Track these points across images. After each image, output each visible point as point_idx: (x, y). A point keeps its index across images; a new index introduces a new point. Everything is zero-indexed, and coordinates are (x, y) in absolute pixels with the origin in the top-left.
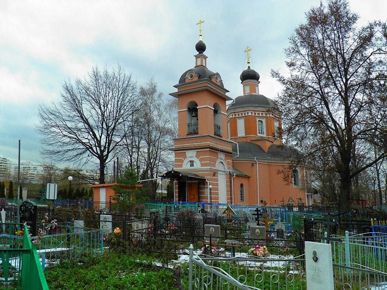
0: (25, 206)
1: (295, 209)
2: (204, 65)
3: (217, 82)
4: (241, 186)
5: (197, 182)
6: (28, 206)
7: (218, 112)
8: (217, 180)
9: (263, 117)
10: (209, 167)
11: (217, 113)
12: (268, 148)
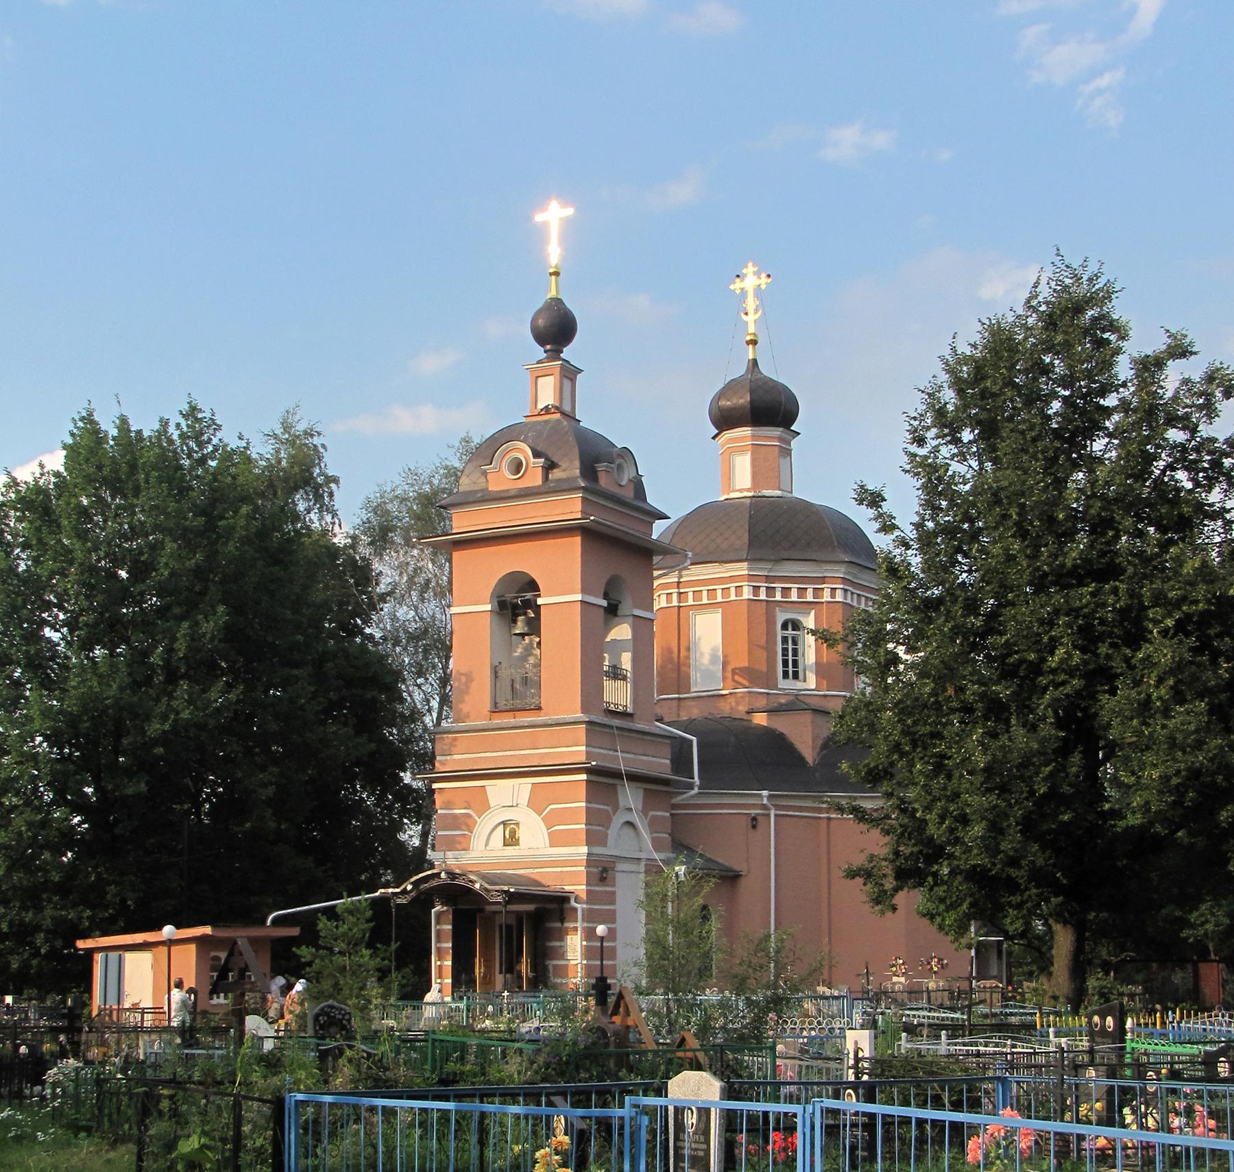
0: (327, 1014)
3: (620, 485)
5: (531, 907)
7: (619, 613)
11: (616, 615)
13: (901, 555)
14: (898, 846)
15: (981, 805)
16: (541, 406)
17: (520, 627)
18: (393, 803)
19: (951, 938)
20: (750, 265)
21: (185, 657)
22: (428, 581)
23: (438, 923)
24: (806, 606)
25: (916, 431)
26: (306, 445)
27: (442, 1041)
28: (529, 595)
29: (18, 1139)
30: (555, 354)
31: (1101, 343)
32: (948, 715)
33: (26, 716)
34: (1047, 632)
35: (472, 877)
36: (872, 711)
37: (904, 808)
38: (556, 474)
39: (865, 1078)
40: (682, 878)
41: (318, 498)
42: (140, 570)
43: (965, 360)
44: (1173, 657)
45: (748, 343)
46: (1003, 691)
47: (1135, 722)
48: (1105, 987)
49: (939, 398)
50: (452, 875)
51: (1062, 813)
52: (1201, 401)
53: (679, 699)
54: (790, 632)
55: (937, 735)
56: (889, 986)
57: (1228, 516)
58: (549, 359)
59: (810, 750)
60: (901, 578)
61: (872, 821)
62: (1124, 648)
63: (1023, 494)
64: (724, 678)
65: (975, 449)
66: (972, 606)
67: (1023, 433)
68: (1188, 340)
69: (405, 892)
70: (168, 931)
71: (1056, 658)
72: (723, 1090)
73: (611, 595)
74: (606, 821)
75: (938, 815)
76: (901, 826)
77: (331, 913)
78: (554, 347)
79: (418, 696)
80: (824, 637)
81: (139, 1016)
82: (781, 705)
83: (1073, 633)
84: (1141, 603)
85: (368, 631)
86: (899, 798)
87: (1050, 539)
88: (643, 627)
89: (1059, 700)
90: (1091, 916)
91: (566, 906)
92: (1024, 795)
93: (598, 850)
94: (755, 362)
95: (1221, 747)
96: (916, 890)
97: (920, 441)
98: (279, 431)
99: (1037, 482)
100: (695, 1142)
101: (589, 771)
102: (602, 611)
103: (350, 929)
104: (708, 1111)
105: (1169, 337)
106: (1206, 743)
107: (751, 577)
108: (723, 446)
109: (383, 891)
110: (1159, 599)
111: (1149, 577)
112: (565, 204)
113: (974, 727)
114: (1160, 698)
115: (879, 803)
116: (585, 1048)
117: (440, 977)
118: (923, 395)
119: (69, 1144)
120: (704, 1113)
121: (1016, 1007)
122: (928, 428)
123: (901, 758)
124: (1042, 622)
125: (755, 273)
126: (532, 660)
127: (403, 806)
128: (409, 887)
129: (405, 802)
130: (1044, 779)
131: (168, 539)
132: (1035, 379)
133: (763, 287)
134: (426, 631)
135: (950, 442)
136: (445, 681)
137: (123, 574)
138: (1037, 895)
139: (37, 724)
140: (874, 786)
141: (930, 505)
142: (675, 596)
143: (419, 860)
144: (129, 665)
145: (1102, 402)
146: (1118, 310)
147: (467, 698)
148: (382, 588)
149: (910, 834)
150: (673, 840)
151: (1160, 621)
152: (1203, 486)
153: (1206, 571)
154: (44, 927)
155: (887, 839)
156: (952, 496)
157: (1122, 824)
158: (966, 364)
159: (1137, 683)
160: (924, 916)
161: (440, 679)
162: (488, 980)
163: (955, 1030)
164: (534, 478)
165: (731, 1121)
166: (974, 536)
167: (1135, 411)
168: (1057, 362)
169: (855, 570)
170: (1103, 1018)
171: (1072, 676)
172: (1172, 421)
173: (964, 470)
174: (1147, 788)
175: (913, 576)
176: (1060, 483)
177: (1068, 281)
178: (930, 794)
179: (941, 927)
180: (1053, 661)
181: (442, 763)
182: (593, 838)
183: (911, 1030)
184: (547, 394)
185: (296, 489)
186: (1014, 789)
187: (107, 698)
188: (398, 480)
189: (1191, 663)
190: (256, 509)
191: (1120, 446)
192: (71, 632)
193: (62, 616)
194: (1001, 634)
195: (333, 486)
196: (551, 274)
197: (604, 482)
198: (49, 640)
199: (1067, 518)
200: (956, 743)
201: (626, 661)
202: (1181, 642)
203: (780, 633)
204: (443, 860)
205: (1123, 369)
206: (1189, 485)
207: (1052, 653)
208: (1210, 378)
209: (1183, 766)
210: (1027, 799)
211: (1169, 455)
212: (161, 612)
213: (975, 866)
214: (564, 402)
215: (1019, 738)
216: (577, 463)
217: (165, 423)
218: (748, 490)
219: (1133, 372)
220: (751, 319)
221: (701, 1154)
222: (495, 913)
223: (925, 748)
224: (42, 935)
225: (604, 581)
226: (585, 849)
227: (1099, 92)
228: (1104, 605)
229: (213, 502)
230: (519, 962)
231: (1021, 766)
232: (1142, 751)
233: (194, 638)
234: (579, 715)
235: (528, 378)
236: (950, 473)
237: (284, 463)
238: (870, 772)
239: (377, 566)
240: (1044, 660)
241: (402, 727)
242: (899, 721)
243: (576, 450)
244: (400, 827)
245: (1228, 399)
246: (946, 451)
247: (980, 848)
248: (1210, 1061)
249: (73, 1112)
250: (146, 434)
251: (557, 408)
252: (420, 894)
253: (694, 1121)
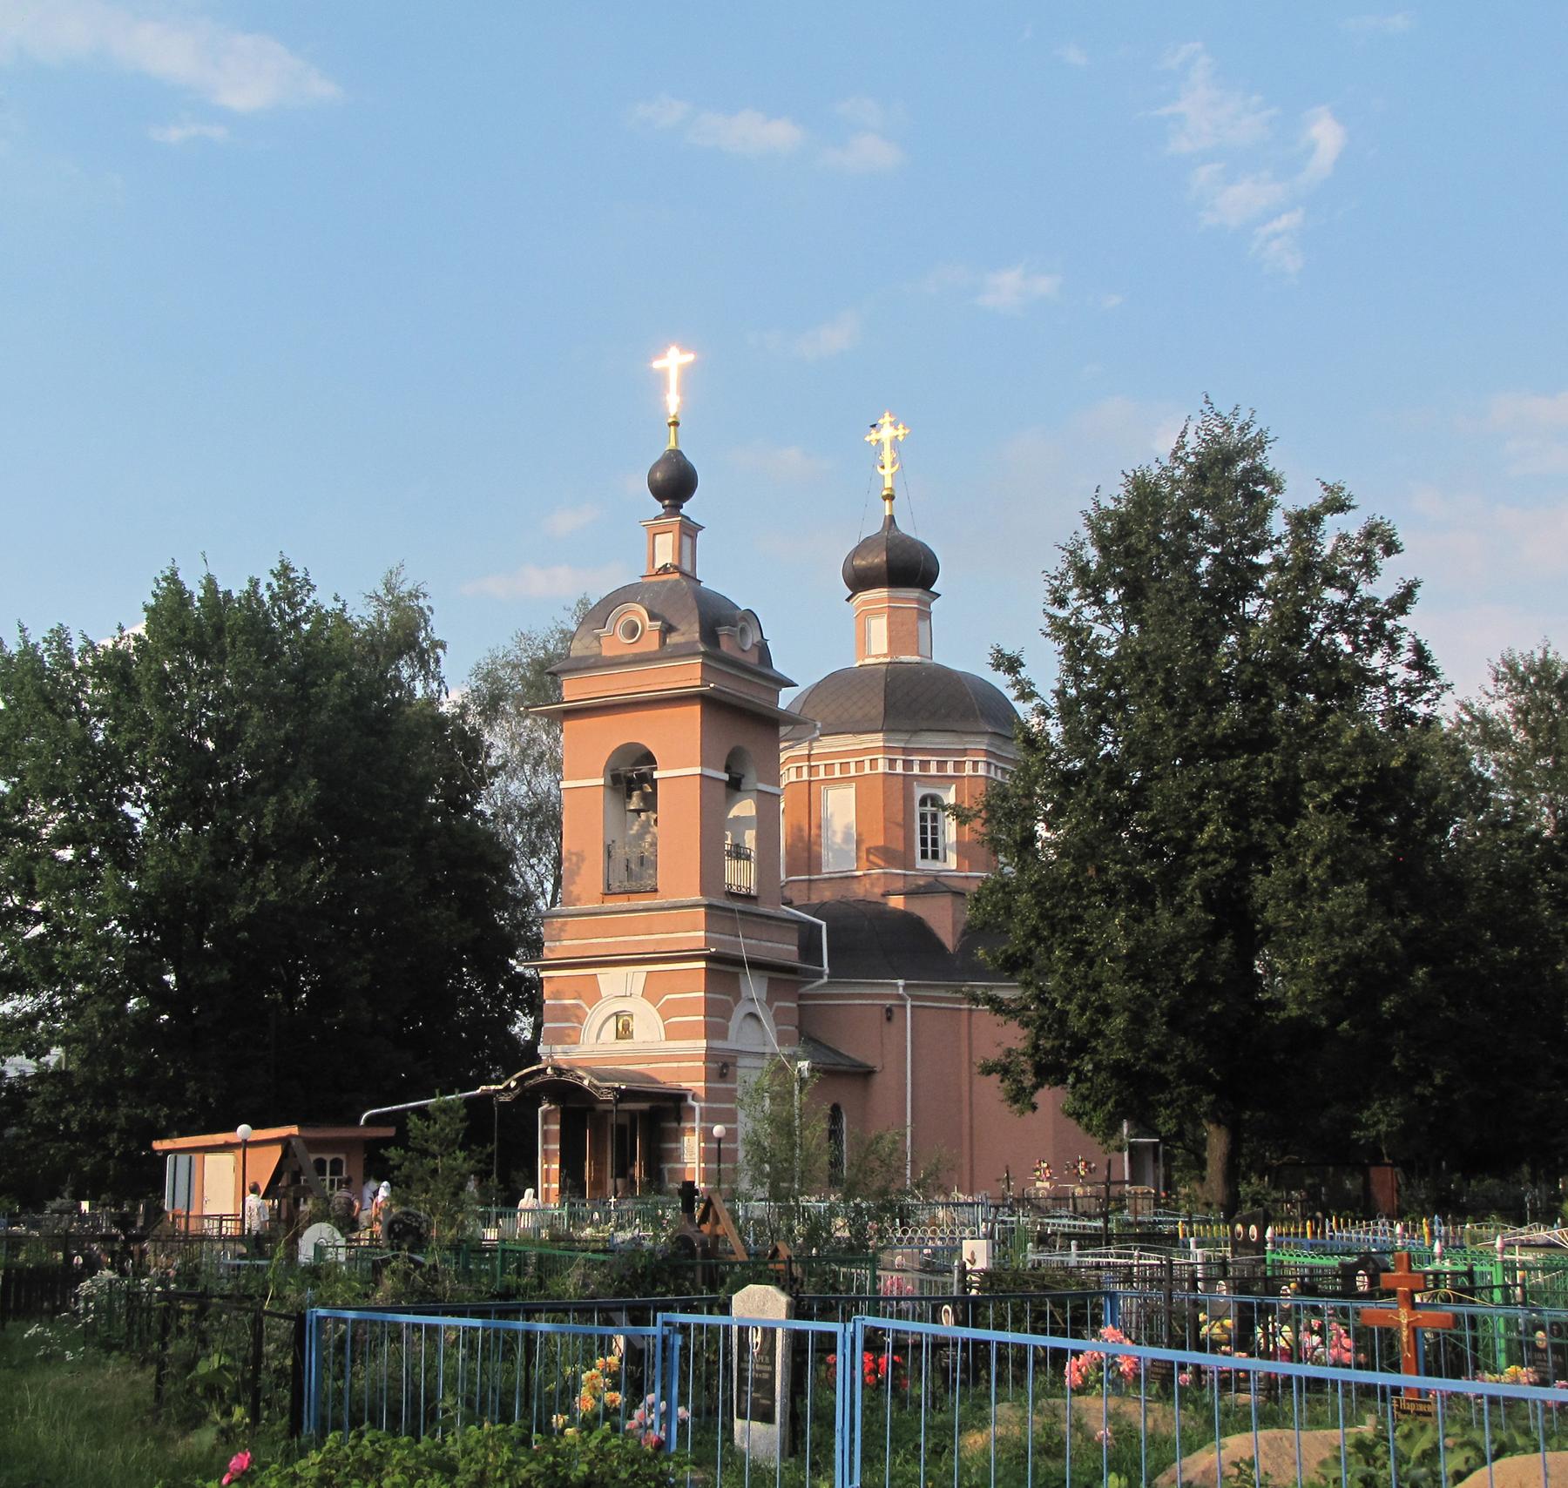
1: (466, 1452)
5: (644, 1106)
7: (742, 787)
13: (1039, 724)
14: (1038, 1039)
15: (1124, 994)
16: (658, 565)
17: (635, 803)
18: (504, 993)
19: (1099, 1139)
20: (887, 414)
21: (273, 834)
22: (542, 754)
23: (545, 1122)
24: (944, 780)
25: (1056, 591)
26: (410, 607)
27: (511, 1251)
28: (645, 769)
29: (46, 1358)
30: (674, 509)
31: (1252, 497)
32: (1089, 897)
33: (100, 898)
34: (1195, 808)
35: (580, 1073)
36: (1010, 893)
37: (1041, 998)
38: (673, 639)
39: (974, 1292)
40: (806, 1074)
41: (424, 664)
42: (228, 740)
43: (1107, 515)
44: (1330, 834)
45: (885, 498)
46: (1148, 871)
47: (1290, 905)
48: (1259, 1193)
49: (1081, 556)
50: (558, 1070)
51: (1211, 1004)
52: (1360, 558)
53: (810, 881)
54: (929, 808)
55: (1076, 919)
56: (1033, 1192)
57: (1391, 682)
58: (668, 515)
59: (950, 937)
60: (1039, 749)
61: (1010, 1012)
62: (1276, 825)
63: (1168, 658)
64: (858, 858)
65: (1120, 611)
66: (1117, 779)
67: (1169, 593)
68: (1346, 493)
69: (508, 1088)
70: (243, 1130)
71: (1205, 836)
72: (789, 1306)
73: (734, 769)
74: (726, 1013)
75: (1079, 1006)
76: (1040, 1017)
77: (422, 1112)
78: (673, 502)
79: (531, 878)
80: (962, 816)
81: (216, 1224)
82: (919, 887)
83: (1223, 809)
84: (1297, 776)
85: (478, 807)
86: (1038, 987)
87: (1199, 708)
88: (768, 803)
89: (1206, 880)
90: (1247, 1115)
91: (683, 1104)
92: (1171, 984)
93: (718, 1044)
94: (891, 519)
95: (1382, 932)
96: (1059, 1087)
97: (1061, 602)
98: (382, 592)
99: (1185, 648)
100: (760, 1363)
101: (708, 958)
102: (723, 785)
103: (442, 1129)
104: (773, 1331)
105: (1326, 489)
106: (1366, 927)
107: (886, 749)
108: (857, 608)
109: (484, 1087)
110: (1317, 772)
111: (1307, 747)
112: (684, 348)
113: (1117, 910)
114: (1316, 879)
115: (1017, 993)
116: (664, 1259)
117: (547, 1181)
118: (1064, 553)
119: (97, 1364)
120: (769, 1333)
121: (1166, 1214)
122: (1070, 589)
123: (1038, 944)
124: (1191, 797)
125: (892, 424)
126: (649, 838)
127: (515, 997)
128: (513, 1084)
129: (517, 992)
130: (1192, 967)
131: (255, 708)
132: (1182, 536)
133: (901, 438)
134: (540, 806)
135: (1093, 603)
136: (558, 862)
137: (210, 745)
138: (1188, 1093)
139: (110, 908)
140: (1013, 974)
141: (1074, 671)
142: (805, 770)
143: (529, 1053)
144: (211, 843)
145: (1255, 559)
146: (1272, 460)
147: (578, 879)
148: (492, 762)
149: (1050, 1026)
150: (801, 1034)
151: (1315, 795)
152: (1363, 650)
153: (1366, 742)
154: (118, 1127)
155: (1026, 1031)
156: (1096, 661)
157: (1283, 1015)
158: (1109, 520)
159: (1292, 861)
160: (1070, 1115)
161: (554, 859)
162: (598, 1184)
163: (1088, 1240)
164: (651, 643)
165: (797, 1341)
166: (1120, 704)
167: (1290, 569)
168: (1206, 517)
169: (998, 742)
170: (1246, 1227)
171: (1223, 855)
172: (1330, 580)
173: (1107, 634)
174: (1302, 977)
175: (1052, 748)
176: (1210, 646)
177: (1218, 431)
178: (1070, 983)
179: (1088, 1128)
180: (1203, 838)
181: (551, 950)
182: (714, 1030)
183: (1043, 1240)
184: (665, 551)
185: (399, 655)
186: (1159, 978)
187: (188, 879)
188: (510, 645)
189: (1351, 840)
190: (352, 676)
191: (1276, 606)
192: (155, 807)
193: (144, 791)
194: (1148, 809)
195: (439, 651)
196: (670, 425)
197: (726, 646)
198: (126, 817)
199: (1216, 685)
200: (1098, 927)
201: (750, 839)
202: (1339, 818)
203: (918, 810)
204: (553, 1054)
205: (1277, 525)
206: (1348, 649)
207: (1201, 831)
208: (1369, 534)
209: (1340, 952)
210: (1173, 988)
211: (1327, 617)
212: (250, 786)
213: (1118, 1061)
214: (684, 561)
215: (1165, 923)
216: (696, 627)
217: (255, 583)
218: (885, 656)
219: (1288, 527)
220: (887, 472)
221: (766, 1376)
222: (606, 1112)
223: (1064, 933)
224: (115, 1135)
225: (727, 751)
226: (703, 1043)
227: (1277, 235)
228: (1257, 778)
229: (305, 669)
230: (633, 1165)
231: (1165, 953)
232: (1298, 936)
233: (280, 812)
234: (698, 898)
235: (644, 534)
236: (1093, 636)
237: (387, 626)
238: (1008, 959)
239: (487, 737)
240: (1192, 838)
241: (514, 910)
242: (1036, 904)
243: (696, 612)
244: (511, 1019)
245: (1389, 555)
246: (1090, 612)
247: (1122, 1042)
248: (1348, 1273)
249: (106, 1328)
250: (235, 595)
251: (676, 567)
252: (525, 1091)
253: (759, 1340)
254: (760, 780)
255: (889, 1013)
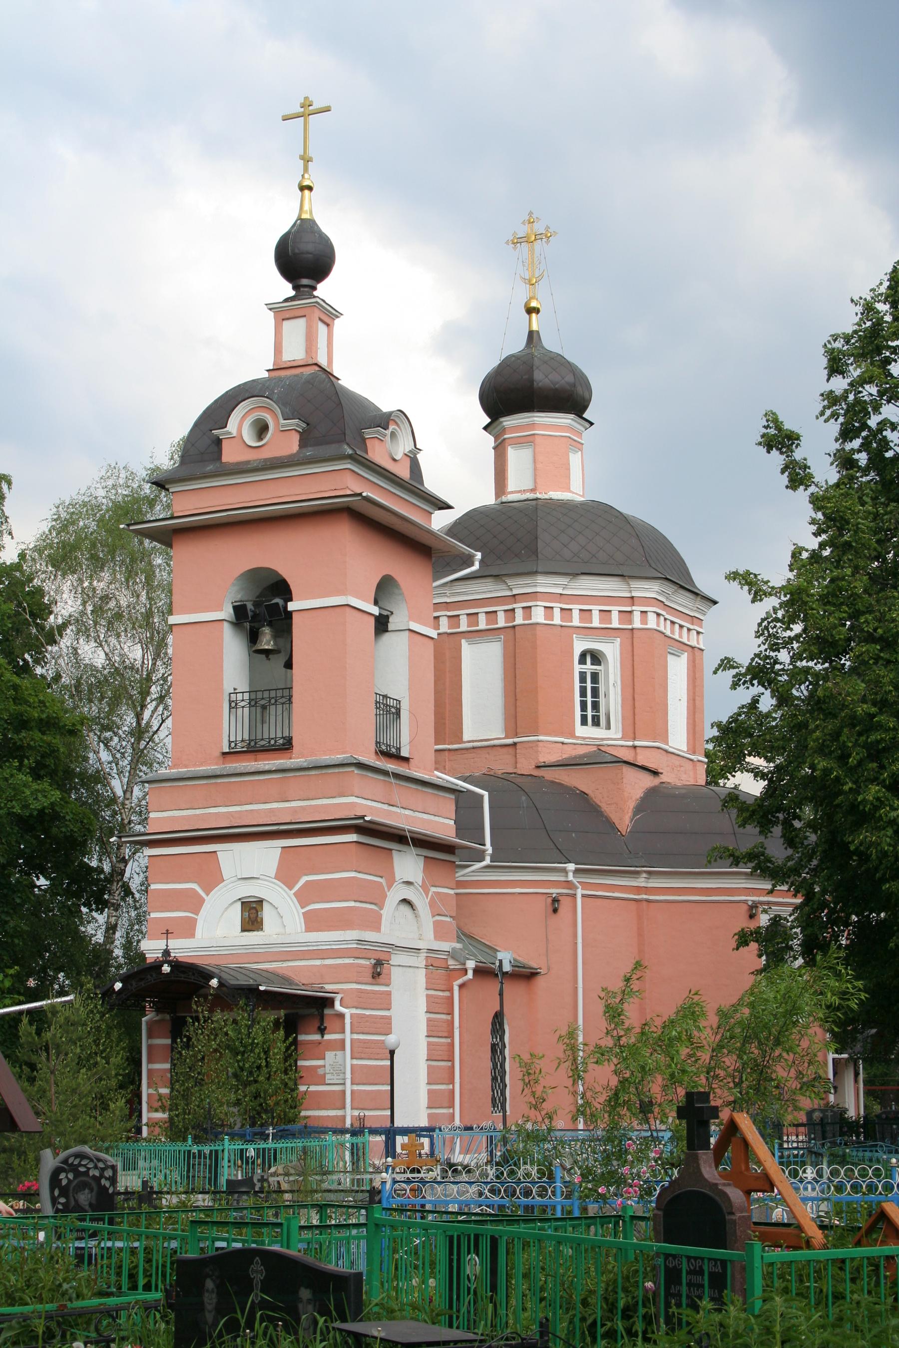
0: (74, 1169)
2: (323, 362)
3: (395, 460)
4: (493, 1024)
6: (89, 1169)
7: (391, 627)
8: (385, 1002)
9: (608, 632)
10: (352, 934)
11: (386, 631)
12: (631, 805)
102: (372, 621)
254: (411, 618)
255: (555, 904)
